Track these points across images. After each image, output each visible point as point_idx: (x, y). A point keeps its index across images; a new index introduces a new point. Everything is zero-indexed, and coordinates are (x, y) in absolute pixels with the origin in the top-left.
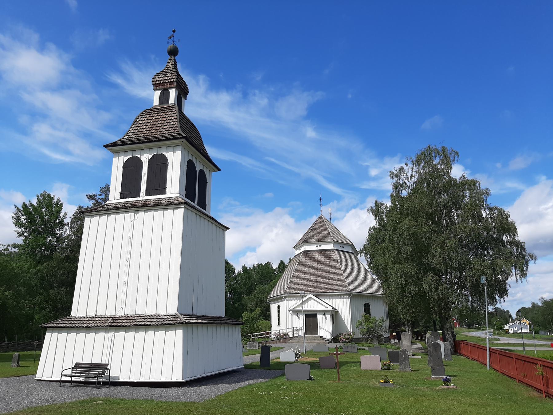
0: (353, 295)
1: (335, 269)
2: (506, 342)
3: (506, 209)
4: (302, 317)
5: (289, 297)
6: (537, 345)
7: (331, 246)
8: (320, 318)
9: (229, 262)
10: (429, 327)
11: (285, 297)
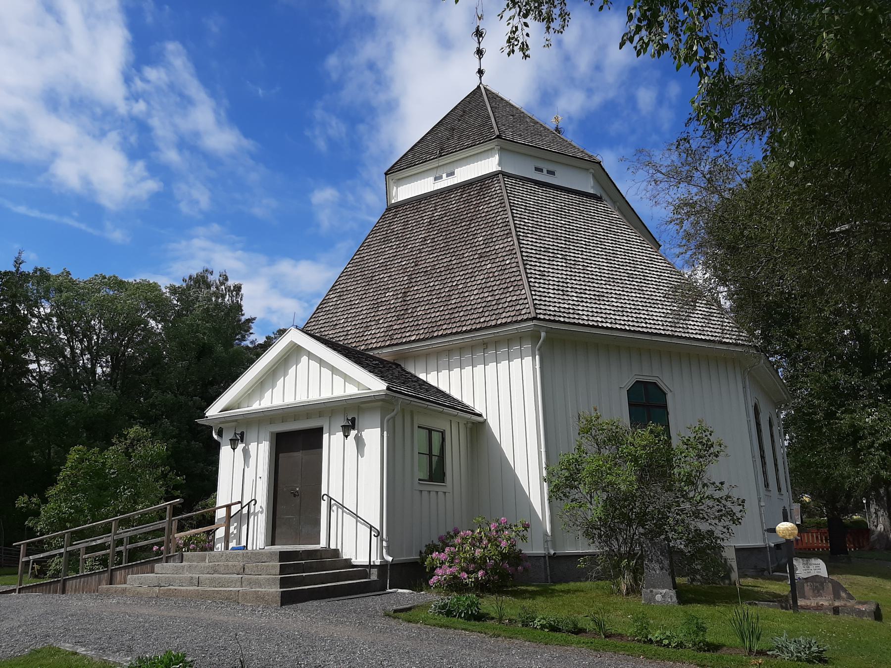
8: (334, 445)
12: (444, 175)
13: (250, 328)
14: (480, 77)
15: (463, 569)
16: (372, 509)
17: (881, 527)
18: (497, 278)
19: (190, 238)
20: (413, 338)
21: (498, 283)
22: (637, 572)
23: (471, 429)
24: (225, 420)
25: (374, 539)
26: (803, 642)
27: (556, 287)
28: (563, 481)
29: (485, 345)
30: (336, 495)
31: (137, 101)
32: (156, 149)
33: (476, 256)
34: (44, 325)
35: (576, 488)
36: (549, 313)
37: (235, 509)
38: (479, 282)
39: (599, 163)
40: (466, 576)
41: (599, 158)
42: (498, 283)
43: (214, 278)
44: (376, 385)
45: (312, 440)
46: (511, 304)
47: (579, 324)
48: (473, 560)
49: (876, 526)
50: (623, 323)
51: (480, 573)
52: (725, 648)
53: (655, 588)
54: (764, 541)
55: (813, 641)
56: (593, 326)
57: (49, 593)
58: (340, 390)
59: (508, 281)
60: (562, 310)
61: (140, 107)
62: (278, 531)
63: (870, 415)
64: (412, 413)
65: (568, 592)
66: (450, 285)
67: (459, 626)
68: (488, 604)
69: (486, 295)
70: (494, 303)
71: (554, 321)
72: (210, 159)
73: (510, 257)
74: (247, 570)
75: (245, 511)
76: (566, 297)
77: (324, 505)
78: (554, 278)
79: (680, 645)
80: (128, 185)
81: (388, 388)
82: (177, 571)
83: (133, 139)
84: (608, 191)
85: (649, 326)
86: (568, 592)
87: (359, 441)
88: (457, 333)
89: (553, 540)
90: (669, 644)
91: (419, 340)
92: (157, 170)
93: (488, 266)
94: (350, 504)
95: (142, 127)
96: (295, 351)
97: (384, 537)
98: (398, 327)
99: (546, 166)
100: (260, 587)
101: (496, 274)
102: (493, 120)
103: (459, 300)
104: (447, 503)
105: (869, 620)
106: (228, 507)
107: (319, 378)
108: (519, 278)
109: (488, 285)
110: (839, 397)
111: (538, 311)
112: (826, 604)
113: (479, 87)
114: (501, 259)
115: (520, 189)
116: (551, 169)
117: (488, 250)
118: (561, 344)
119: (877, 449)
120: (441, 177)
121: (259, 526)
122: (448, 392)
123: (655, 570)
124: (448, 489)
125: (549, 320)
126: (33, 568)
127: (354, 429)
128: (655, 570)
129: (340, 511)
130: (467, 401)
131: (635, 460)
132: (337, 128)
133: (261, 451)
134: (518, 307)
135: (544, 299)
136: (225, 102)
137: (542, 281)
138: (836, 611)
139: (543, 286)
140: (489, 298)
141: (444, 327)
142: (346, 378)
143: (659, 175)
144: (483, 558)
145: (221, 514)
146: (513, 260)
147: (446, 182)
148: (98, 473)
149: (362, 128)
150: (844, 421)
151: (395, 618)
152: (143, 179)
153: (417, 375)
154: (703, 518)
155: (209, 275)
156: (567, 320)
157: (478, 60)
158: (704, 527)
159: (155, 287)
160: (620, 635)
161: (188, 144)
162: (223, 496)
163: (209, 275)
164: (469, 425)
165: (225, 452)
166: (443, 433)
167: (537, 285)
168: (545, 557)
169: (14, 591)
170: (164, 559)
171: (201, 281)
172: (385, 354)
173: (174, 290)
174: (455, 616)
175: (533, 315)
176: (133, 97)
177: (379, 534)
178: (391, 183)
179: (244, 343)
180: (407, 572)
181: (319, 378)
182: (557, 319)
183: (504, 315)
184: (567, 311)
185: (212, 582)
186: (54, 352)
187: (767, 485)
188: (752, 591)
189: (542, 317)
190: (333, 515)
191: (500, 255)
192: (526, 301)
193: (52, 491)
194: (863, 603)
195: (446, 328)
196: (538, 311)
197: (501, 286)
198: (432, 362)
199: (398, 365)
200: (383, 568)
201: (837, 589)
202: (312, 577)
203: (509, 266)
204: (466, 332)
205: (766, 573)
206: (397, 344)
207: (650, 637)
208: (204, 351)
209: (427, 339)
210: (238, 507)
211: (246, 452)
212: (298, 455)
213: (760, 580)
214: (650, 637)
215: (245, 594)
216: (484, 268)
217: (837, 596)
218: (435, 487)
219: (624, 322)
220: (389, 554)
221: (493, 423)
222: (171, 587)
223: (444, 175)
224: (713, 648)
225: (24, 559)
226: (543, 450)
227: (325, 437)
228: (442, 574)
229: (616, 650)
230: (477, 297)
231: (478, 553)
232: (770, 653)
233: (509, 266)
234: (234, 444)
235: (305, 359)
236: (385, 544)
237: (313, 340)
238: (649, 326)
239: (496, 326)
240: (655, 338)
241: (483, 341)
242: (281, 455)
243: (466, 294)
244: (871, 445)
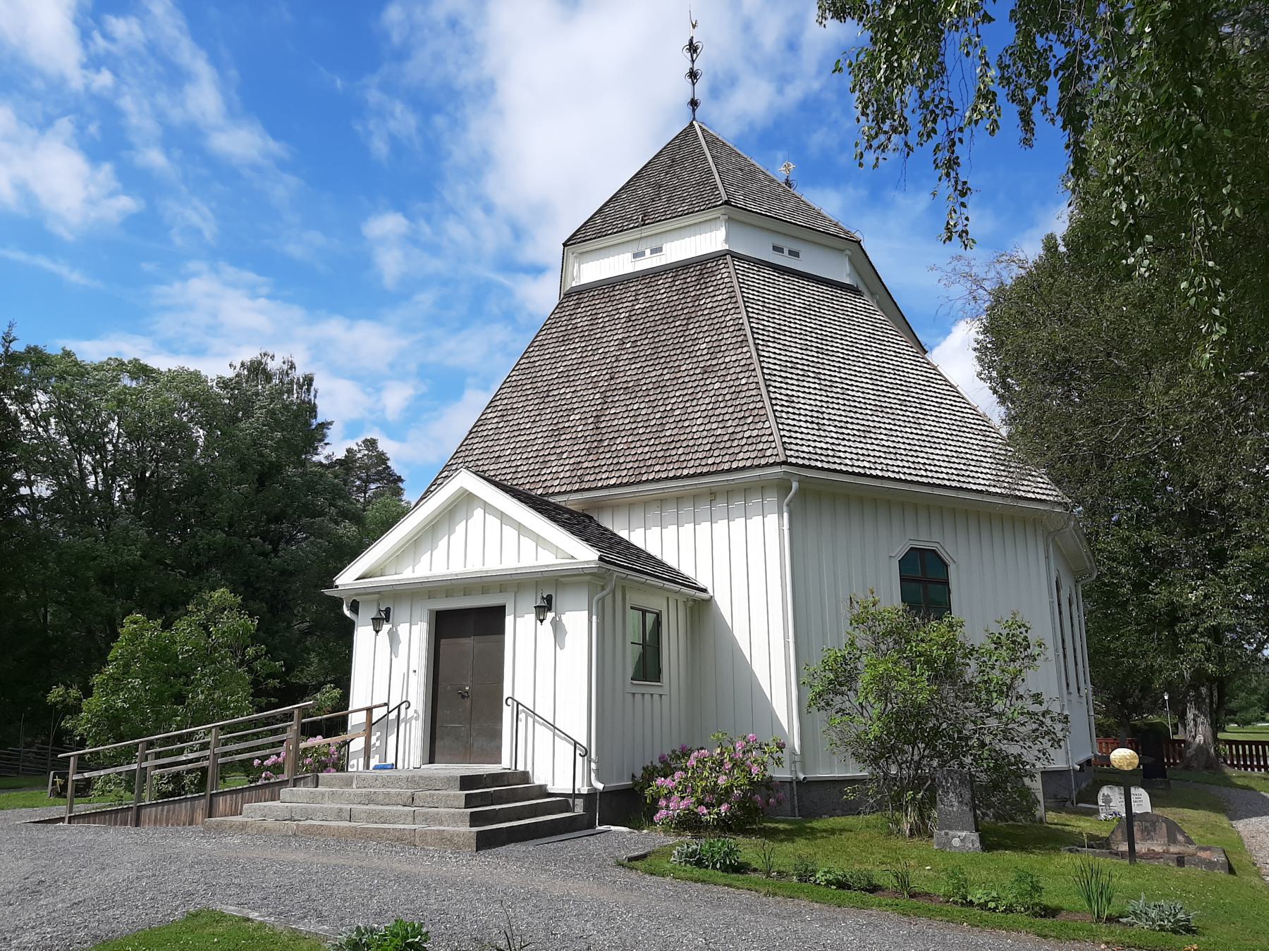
8: (521, 629)
12: (648, 252)
13: (324, 436)
14: (694, 110)
15: (700, 802)
16: (576, 716)
17: (1200, 739)
18: (729, 404)
19: (185, 278)
20: (612, 482)
21: (731, 410)
22: (925, 807)
23: (692, 609)
24: (366, 592)
25: (579, 759)
26: (1166, 907)
27: (809, 419)
28: (826, 685)
29: (713, 495)
30: (524, 697)
31: (98, 71)
32: (130, 147)
33: (698, 371)
34: (40, 430)
35: (843, 694)
36: (802, 455)
38: (703, 408)
39: (859, 242)
40: (705, 811)
41: (858, 236)
42: (731, 410)
43: (273, 366)
44: (586, 555)
45: (489, 622)
46: (750, 441)
47: (841, 471)
48: (714, 789)
49: (1194, 738)
50: (896, 469)
51: (724, 808)
52: (1064, 913)
53: (951, 829)
54: (1068, 761)
55: (1179, 906)
56: (859, 474)
57: (115, 824)
59: (745, 408)
60: (819, 451)
61: (104, 79)
62: (438, 744)
63: (1194, 589)
64: (624, 588)
65: (832, 831)
66: (662, 409)
67: (719, 881)
68: (748, 849)
69: (715, 426)
70: (726, 438)
71: (810, 467)
72: (221, 171)
73: (747, 374)
74: (417, 801)
75: (393, 716)
76: (822, 433)
77: (507, 712)
78: (805, 403)
79: (1009, 909)
80: (90, 201)
81: (601, 559)
82: (313, 799)
83: (93, 129)
84: (868, 284)
85: (929, 474)
86: (832, 831)
87: (557, 627)
88: (675, 478)
89: (802, 761)
90: (996, 908)
91: (621, 485)
92: (132, 178)
93: (716, 386)
94: (544, 710)
95: (107, 108)
96: (466, 500)
97: (593, 756)
98: (590, 465)
99: (788, 245)
100: (441, 824)
101: (727, 397)
102: (717, 176)
103: (676, 431)
104: (662, 712)
105: (1222, 874)
106: (369, 710)
107: (496, 540)
108: (760, 405)
109: (717, 412)
110: (1151, 566)
111: (788, 453)
112: (1159, 849)
113: (691, 125)
114: (734, 377)
115: (756, 277)
116: (795, 247)
117: (714, 362)
118: (818, 497)
119: (1202, 635)
120: (643, 254)
121: (414, 734)
122: (659, 557)
123: (952, 803)
124: (665, 691)
125: (803, 466)
126: (54, 783)
127: (550, 610)
128: (952, 803)
129: (530, 720)
130: (687, 570)
132: (404, 120)
133: (414, 635)
134: (760, 446)
135: (794, 435)
136: (233, 73)
137: (790, 410)
138: (1180, 861)
139: (792, 416)
140: (719, 431)
141: (657, 468)
142: (539, 540)
143: (981, 291)
144: (728, 790)
145: (356, 719)
146: (751, 380)
147: (649, 262)
148: (162, 653)
149: (439, 121)
150: (1159, 596)
151: (632, 869)
152: (112, 194)
153: (616, 531)
154: (1012, 739)
155: (269, 361)
156: (826, 465)
157: (690, 86)
158: (1014, 749)
159: (196, 377)
160: (927, 894)
161: (185, 140)
162: (359, 696)
163: (269, 361)
164: (691, 603)
165: (363, 636)
166: (658, 616)
167: (784, 415)
168: (791, 782)
169: (62, 819)
170: (291, 782)
171: (257, 370)
172: (572, 501)
173: (224, 384)
174: (707, 867)
175: (782, 458)
176: (94, 63)
177: (587, 753)
178: (571, 258)
179: (316, 458)
180: (624, 803)
181: (496, 540)
182: (813, 463)
183: (741, 456)
184: (825, 452)
185: (370, 816)
186: (54, 469)
188: (1063, 831)
189: (793, 460)
190: (521, 725)
191: (732, 371)
192: (771, 438)
193: (96, 679)
194: (1205, 849)
195: (659, 470)
196: (788, 453)
197: (735, 415)
198: (638, 516)
199: (591, 518)
200: (590, 798)
201: (1173, 831)
202: (508, 815)
203: (745, 388)
204: (687, 476)
205: (1068, 804)
206: (589, 489)
207: (969, 898)
208: (266, 475)
209: (633, 483)
210: (384, 710)
211: (393, 637)
212: (469, 643)
213: (1064, 815)
214: (969, 898)
215: (424, 835)
216: (710, 387)
217: (1172, 840)
218: (648, 687)
219: (898, 468)
220: (599, 779)
221: (722, 601)
222: (309, 822)
223: (648, 252)
224: (1051, 912)
226: (791, 640)
227: (509, 620)
228: (677, 806)
229: (930, 914)
230: (702, 428)
231: (722, 781)
232: (1124, 920)
233: (745, 388)
234: (377, 623)
235: (479, 512)
236: (593, 766)
237: (493, 487)
238: (929, 474)
239: (729, 471)
240: (937, 492)
241: (713, 488)
242: (443, 641)
243: (686, 424)
244: (1194, 631)
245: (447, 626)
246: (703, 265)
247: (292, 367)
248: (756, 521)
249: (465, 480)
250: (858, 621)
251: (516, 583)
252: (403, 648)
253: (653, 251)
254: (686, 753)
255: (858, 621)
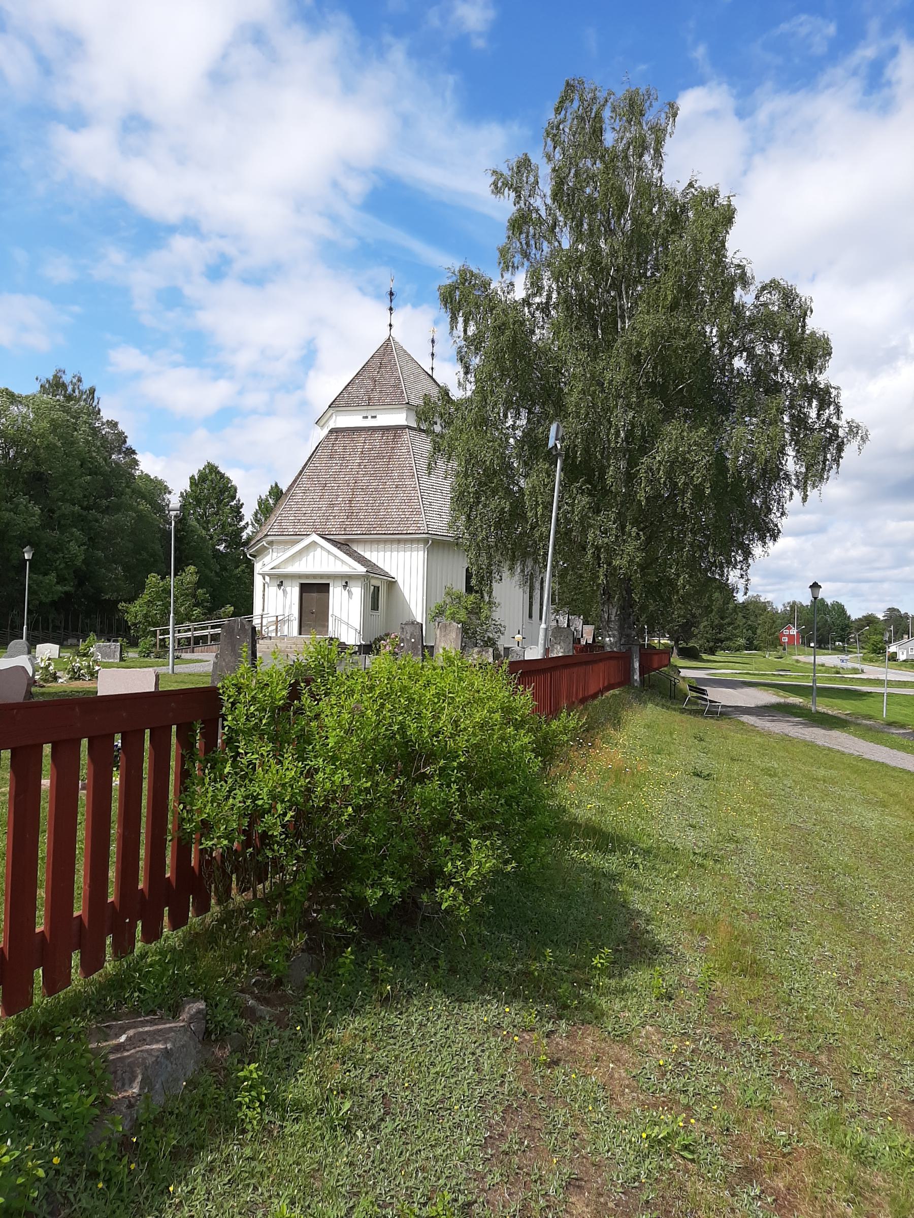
0: (434, 541)
1: (401, 477)
2: (872, 677)
3: (803, 291)
4: (294, 592)
5: (280, 542)
6: (890, 683)
7: (399, 418)
8: (336, 593)
9: (222, 470)
10: (722, 642)
11: (271, 543)
30: (337, 613)
37: (279, 618)
44: (361, 569)
58: (345, 569)
77: (330, 619)
94: (345, 618)
130: (387, 569)
131: (466, 608)
147: (370, 423)
187: (530, 616)
198: (368, 547)
218: (375, 612)
221: (400, 582)
225: (161, 637)
227: (331, 589)
235: (319, 549)
241: (399, 540)
245: (305, 589)
246: (395, 430)
247: (80, 380)
248: (415, 553)
249: (315, 537)
250: (448, 594)
251: (336, 577)
252: (289, 596)
253: (373, 417)
254: (387, 635)
255: (448, 594)
